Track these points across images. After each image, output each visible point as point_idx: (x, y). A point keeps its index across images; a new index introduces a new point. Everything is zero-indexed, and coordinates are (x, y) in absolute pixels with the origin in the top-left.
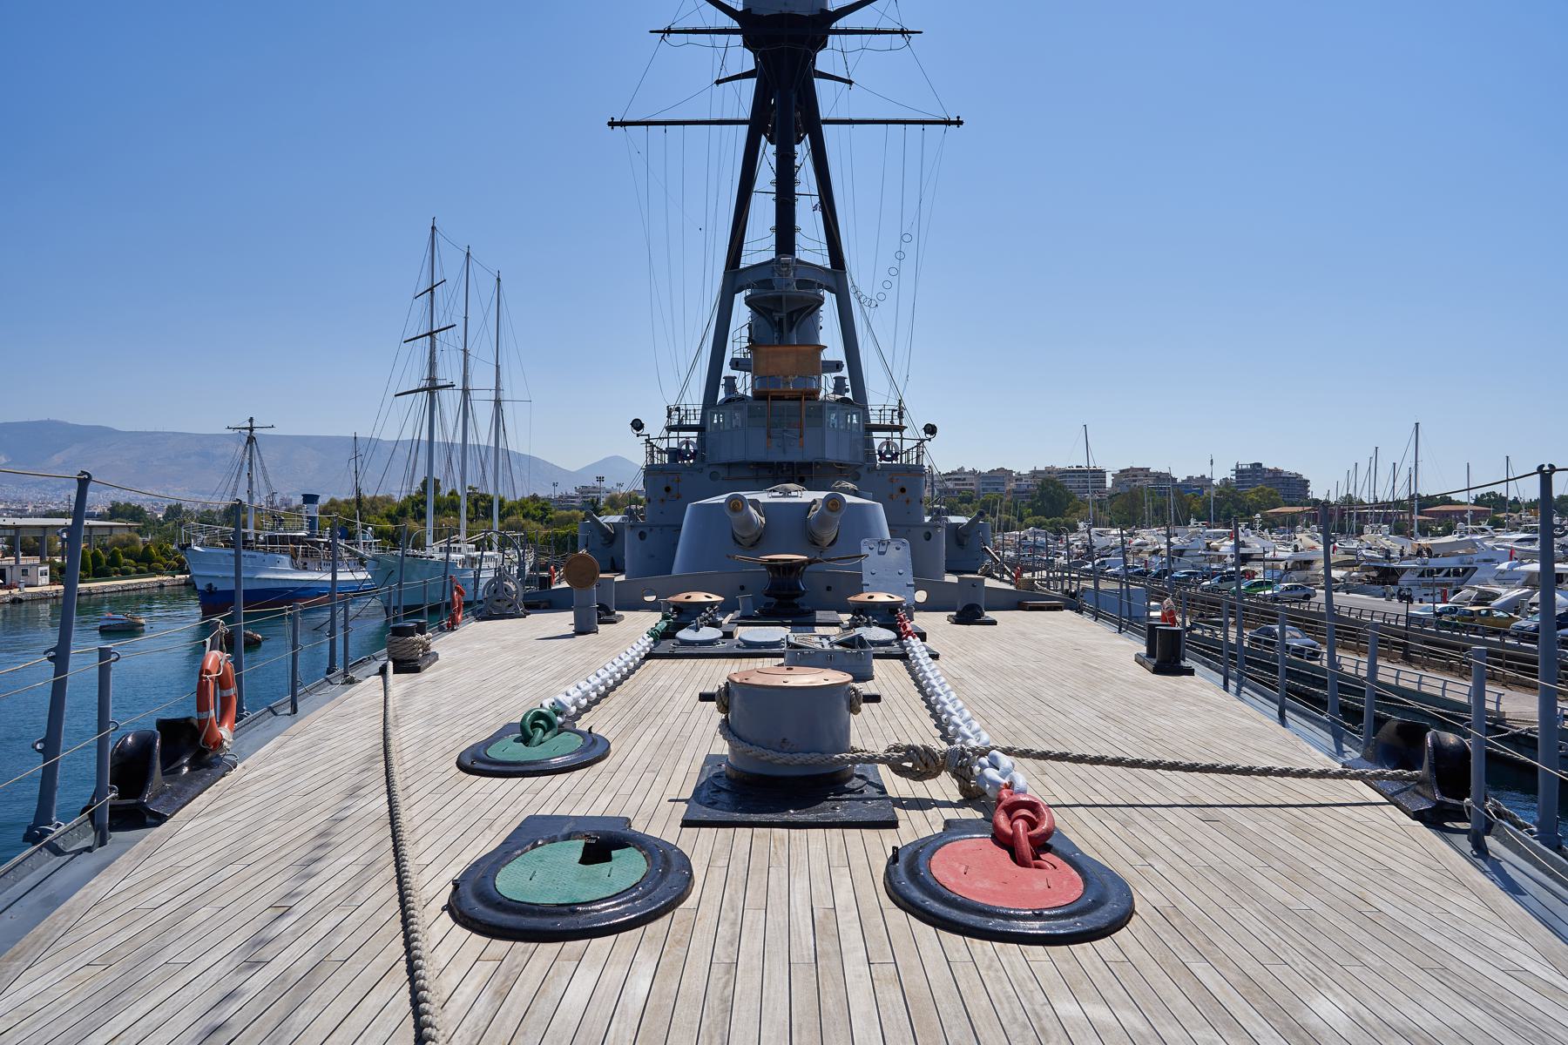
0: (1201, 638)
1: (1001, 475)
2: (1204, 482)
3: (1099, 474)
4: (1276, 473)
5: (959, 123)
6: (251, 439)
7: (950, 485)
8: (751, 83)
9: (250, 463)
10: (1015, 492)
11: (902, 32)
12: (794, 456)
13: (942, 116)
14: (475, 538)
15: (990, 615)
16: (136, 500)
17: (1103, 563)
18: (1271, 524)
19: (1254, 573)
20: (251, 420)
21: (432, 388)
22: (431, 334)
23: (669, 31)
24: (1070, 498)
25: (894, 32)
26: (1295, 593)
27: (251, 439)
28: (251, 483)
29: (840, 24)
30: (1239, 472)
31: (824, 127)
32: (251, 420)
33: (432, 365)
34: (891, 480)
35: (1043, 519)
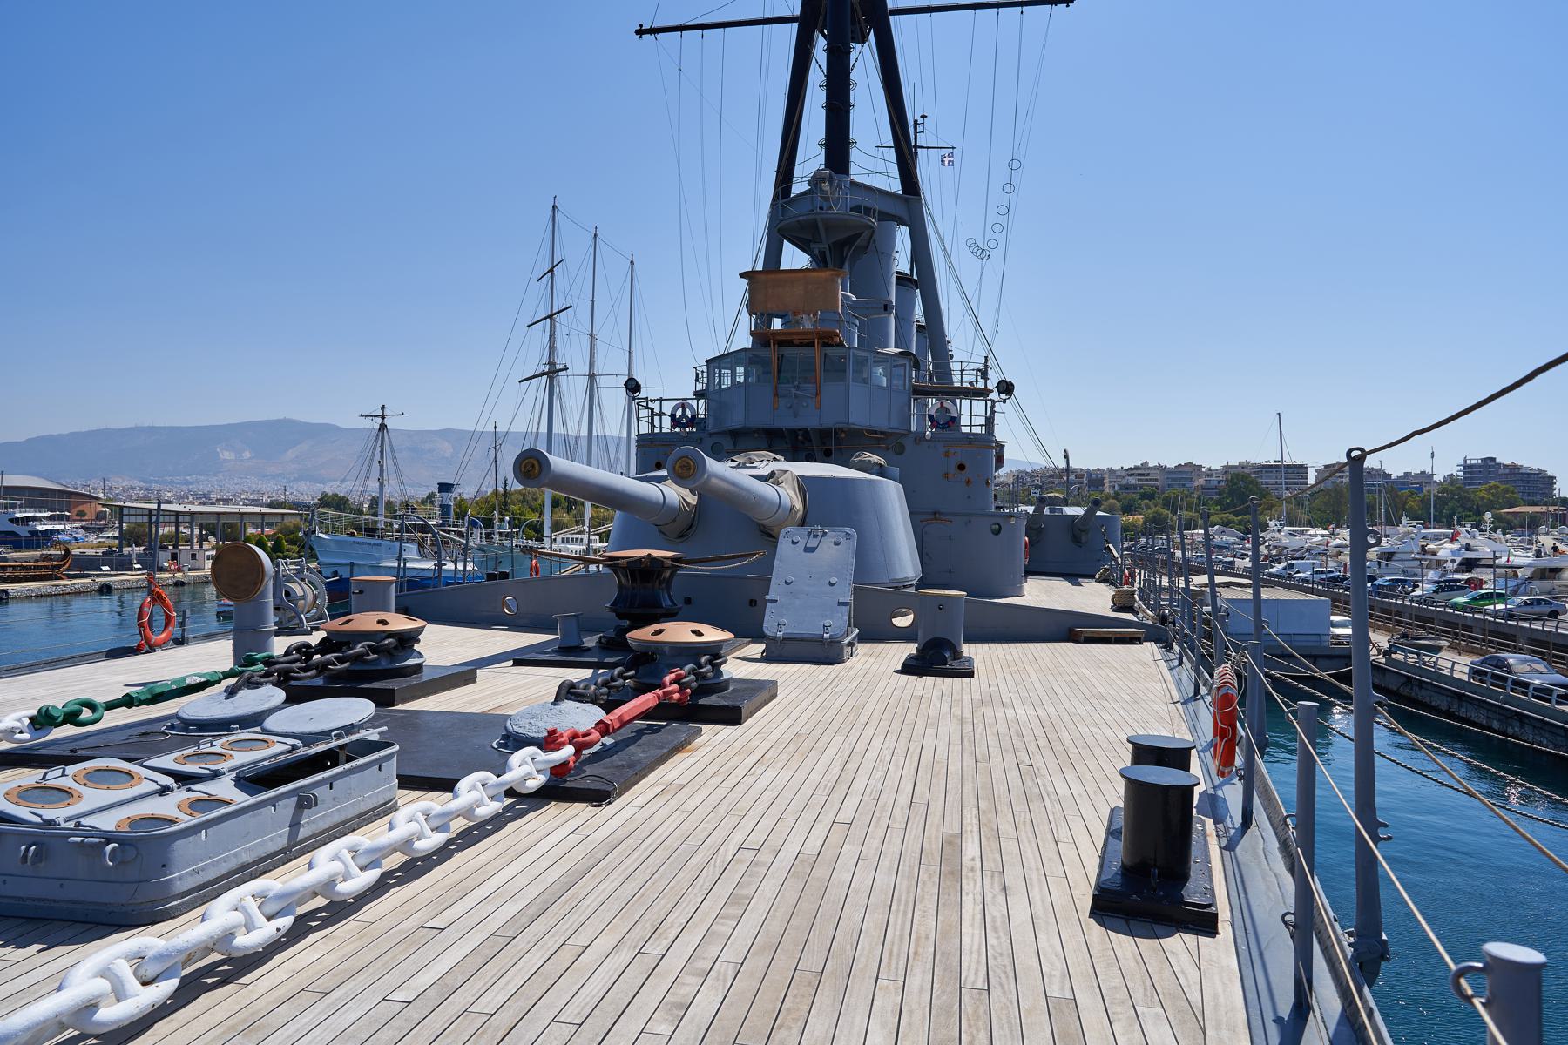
0: (1404, 665)
1: (1189, 470)
2: (1426, 477)
3: (1301, 469)
4: (1514, 469)
6: (383, 427)
7: (1133, 480)
10: (1203, 488)
12: (810, 419)
14: (600, 529)
17: (1291, 566)
18: (1505, 525)
19: (1482, 582)
20: (383, 408)
21: (552, 372)
22: (550, 317)
24: (1263, 494)
26: (1537, 609)
27: (383, 427)
28: (382, 471)
30: (1468, 468)
31: (891, 18)
32: (383, 408)
33: (552, 349)
34: (946, 454)
35: (1232, 517)
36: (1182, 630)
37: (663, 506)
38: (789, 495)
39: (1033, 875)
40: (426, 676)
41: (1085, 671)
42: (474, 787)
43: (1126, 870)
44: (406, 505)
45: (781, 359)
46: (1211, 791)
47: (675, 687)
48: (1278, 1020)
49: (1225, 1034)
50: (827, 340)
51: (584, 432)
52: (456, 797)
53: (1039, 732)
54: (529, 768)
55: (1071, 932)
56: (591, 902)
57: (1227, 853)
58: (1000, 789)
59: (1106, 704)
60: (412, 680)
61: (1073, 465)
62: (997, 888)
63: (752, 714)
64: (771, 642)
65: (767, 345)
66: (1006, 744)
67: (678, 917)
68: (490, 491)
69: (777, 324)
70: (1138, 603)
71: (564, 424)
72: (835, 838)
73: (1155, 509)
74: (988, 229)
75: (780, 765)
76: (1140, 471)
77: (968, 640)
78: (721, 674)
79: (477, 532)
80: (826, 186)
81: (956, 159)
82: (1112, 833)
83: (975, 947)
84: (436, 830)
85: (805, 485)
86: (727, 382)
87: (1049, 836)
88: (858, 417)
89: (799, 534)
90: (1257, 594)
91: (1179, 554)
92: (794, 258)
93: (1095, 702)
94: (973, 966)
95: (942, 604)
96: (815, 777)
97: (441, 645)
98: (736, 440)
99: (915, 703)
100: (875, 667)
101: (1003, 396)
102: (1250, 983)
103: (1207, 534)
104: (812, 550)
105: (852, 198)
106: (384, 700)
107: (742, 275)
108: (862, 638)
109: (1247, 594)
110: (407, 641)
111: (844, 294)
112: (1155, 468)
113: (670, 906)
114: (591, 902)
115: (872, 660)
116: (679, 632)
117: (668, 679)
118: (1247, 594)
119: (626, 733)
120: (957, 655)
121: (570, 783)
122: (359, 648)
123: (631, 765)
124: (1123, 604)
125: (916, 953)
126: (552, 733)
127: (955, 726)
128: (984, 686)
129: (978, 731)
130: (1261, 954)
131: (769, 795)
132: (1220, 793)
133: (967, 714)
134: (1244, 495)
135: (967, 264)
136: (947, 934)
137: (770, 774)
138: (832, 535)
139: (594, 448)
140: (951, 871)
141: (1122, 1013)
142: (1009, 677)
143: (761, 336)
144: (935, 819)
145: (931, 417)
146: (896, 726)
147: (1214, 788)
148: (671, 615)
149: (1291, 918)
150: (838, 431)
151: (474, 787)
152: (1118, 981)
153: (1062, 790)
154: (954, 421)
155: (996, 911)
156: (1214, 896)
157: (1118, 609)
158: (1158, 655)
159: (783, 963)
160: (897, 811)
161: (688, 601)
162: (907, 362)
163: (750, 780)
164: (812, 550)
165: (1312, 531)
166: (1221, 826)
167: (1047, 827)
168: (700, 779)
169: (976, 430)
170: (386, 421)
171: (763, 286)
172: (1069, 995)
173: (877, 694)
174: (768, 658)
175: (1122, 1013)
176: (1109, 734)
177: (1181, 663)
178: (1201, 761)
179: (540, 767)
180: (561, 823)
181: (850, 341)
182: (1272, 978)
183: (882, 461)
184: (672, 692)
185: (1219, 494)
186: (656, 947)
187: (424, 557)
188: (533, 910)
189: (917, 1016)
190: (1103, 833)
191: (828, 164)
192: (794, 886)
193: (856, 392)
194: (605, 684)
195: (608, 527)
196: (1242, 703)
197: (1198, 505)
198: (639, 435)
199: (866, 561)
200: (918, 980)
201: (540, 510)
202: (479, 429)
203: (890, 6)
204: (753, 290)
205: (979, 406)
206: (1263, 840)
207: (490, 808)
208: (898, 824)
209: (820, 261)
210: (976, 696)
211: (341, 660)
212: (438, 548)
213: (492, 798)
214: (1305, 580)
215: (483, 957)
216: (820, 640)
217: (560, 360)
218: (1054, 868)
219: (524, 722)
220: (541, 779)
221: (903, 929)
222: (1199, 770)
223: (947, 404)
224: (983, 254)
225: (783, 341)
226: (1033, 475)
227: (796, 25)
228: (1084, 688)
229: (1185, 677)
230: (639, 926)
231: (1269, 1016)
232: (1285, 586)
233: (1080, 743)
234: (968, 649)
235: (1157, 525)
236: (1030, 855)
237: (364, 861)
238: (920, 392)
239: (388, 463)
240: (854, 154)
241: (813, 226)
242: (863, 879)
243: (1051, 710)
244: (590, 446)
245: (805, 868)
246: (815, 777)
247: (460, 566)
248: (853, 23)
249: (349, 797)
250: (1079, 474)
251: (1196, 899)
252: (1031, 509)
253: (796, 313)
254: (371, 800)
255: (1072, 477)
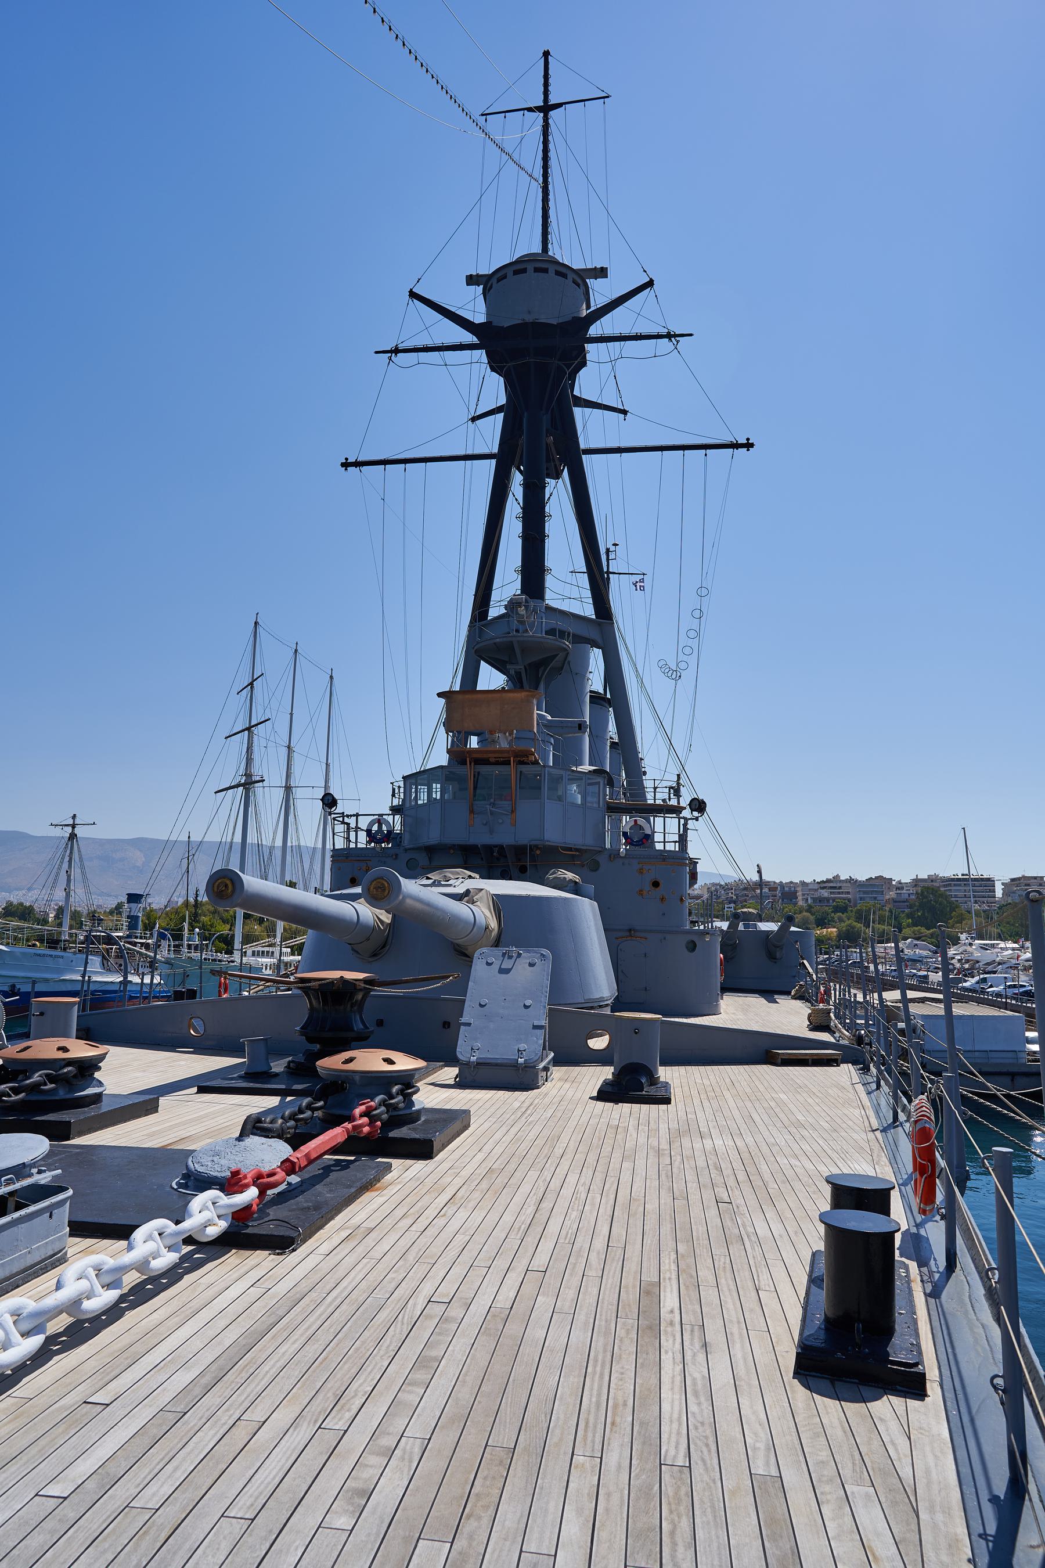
1: (879, 884)
3: (988, 883)
5: (749, 445)
6: (73, 836)
7: (825, 893)
8: (500, 416)
9: (70, 861)
10: (895, 901)
11: (669, 336)
12: (504, 836)
13: (729, 439)
14: (292, 942)
15: (320, 1172)
16: (27, 898)
17: (984, 980)
20: (74, 817)
21: (248, 783)
22: (248, 729)
23: (396, 351)
24: (954, 907)
25: (659, 336)
27: (73, 836)
28: (69, 881)
29: (594, 330)
31: (584, 457)
32: (74, 817)
33: (249, 761)
34: (641, 871)
35: (923, 930)
36: (879, 1050)
37: (357, 925)
38: (484, 914)
39: (734, 1329)
40: (105, 1107)
41: (783, 1096)
42: (149, 1238)
43: (830, 1323)
44: (93, 917)
45: (477, 776)
46: (914, 1230)
47: (365, 1120)
48: (994, 1499)
49: (939, 1517)
50: (523, 758)
51: (279, 843)
52: (130, 1248)
53: (738, 1165)
54: (209, 1214)
55: (775, 1397)
56: (270, 1368)
57: (932, 1301)
58: (699, 1230)
59: (805, 1133)
60: (91, 1111)
61: (766, 877)
62: (697, 1345)
63: (444, 1146)
64: (465, 1067)
65: (463, 762)
66: (705, 1179)
67: (363, 1385)
68: (181, 901)
69: (474, 742)
70: (834, 1022)
71: (258, 830)
72: (529, 1289)
73: (849, 922)
74: (683, 632)
75: (472, 1204)
76: (832, 884)
77: (665, 1063)
78: (412, 1104)
79: (164, 944)
80: (522, 611)
81: (647, 584)
82: (814, 1281)
83: (675, 1416)
84: (108, 1286)
85: (500, 903)
86: (423, 799)
87: (750, 1284)
88: (553, 834)
89: (494, 955)
90: (948, 1009)
91: (872, 967)
92: (490, 678)
93: (793, 1130)
94: (673, 1439)
95: (637, 1027)
96: (508, 1218)
97: (124, 1071)
98: (432, 857)
99: (611, 1134)
100: (570, 1093)
101: (696, 814)
102: (962, 1454)
103: (897, 947)
104: (507, 971)
105: (547, 622)
106: (58, 1132)
107: (440, 695)
108: (557, 1062)
109: (939, 1010)
110: (87, 1068)
111: (539, 713)
112: (846, 881)
113: (354, 1370)
114: (270, 1368)
115: (567, 1085)
116: (370, 1060)
117: (357, 1111)
118: (939, 1010)
119: (314, 1170)
120: (653, 1080)
121: (253, 1228)
122: (36, 1077)
123: (317, 1207)
124: (819, 1024)
125: (613, 1424)
126: (236, 1173)
127: (653, 1160)
128: (681, 1114)
129: (676, 1164)
130: (972, 1421)
131: (461, 1239)
132: (922, 1232)
133: (664, 1146)
134: (935, 908)
135: (659, 686)
136: (648, 1398)
137: (462, 1214)
138: (527, 957)
139: (288, 858)
140: (650, 1328)
141: (830, 1492)
142: (706, 1104)
143: (458, 754)
144: (632, 1266)
145: (625, 834)
146: (592, 1159)
147: (917, 1226)
148: (363, 1041)
149: (999, 1381)
150: (533, 848)
151: (149, 1238)
152: (825, 1454)
153: (762, 1230)
154: (647, 839)
155: (696, 1372)
156: (920, 1353)
157: (815, 1027)
158: (856, 1078)
159: (473, 1439)
160: (593, 1256)
161: (380, 1023)
162: (600, 780)
163: (440, 1222)
164: (507, 971)
165: (1002, 945)
166: (925, 1270)
167: (747, 1273)
168: (389, 1221)
169: (670, 847)
170: (76, 831)
171: (461, 705)
172: (774, 1472)
173: (572, 1123)
174: (462, 1083)
175: (830, 1492)
176: (809, 1166)
177: (879, 1087)
178: (902, 1196)
179: (222, 1212)
180: (243, 1272)
181: (545, 759)
182: (985, 1448)
183: (577, 879)
184: (362, 1126)
185: (911, 907)
186: (337, 1422)
187: (107, 968)
188: (207, 1379)
189: (615, 1499)
190: (805, 1279)
191: (524, 589)
192: (486, 1344)
193: (551, 810)
194: (292, 1117)
195: (300, 940)
196: (939, 1138)
197: (890, 918)
198: (334, 850)
199: (562, 979)
200: (615, 1456)
201: (231, 922)
202: (173, 838)
203: (582, 446)
204: (450, 708)
205: (673, 824)
206: (968, 1288)
207: (167, 1259)
208: (594, 1273)
209: (516, 681)
210: (674, 1125)
211: (16, 1091)
212: (123, 961)
213: (170, 1248)
214: (998, 995)
215: (149, 1439)
216: (515, 1065)
217: (257, 771)
218: (755, 1319)
219: (206, 1160)
220: (223, 1225)
221: (599, 1395)
222: (900, 1213)
223: (641, 821)
224: (675, 675)
225: (479, 759)
226: (727, 888)
227: (494, 461)
228: (782, 1116)
229: (883, 1102)
230: (320, 1396)
231: (984, 1496)
232: (980, 1002)
233: (779, 1177)
234: (665, 1073)
235: (850, 938)
236: (730, 1306)
237: (26, 1326)
238: (615, 809)
239: (76, 873)
240: (549, 581)
241: (509, 647)
242: (557, 1338)
243: (749, 1140)
244: (280, 860)
245: (498, 1321)
246: (508, 1218)
247: (147, 980)
248: (548, 460)
249: (16, 1249)
250: (773, 887)
251: (902, 1357)
252: (724, 925)
253: (492, 732)
254: (39, 1250)
255: (765, 890)
